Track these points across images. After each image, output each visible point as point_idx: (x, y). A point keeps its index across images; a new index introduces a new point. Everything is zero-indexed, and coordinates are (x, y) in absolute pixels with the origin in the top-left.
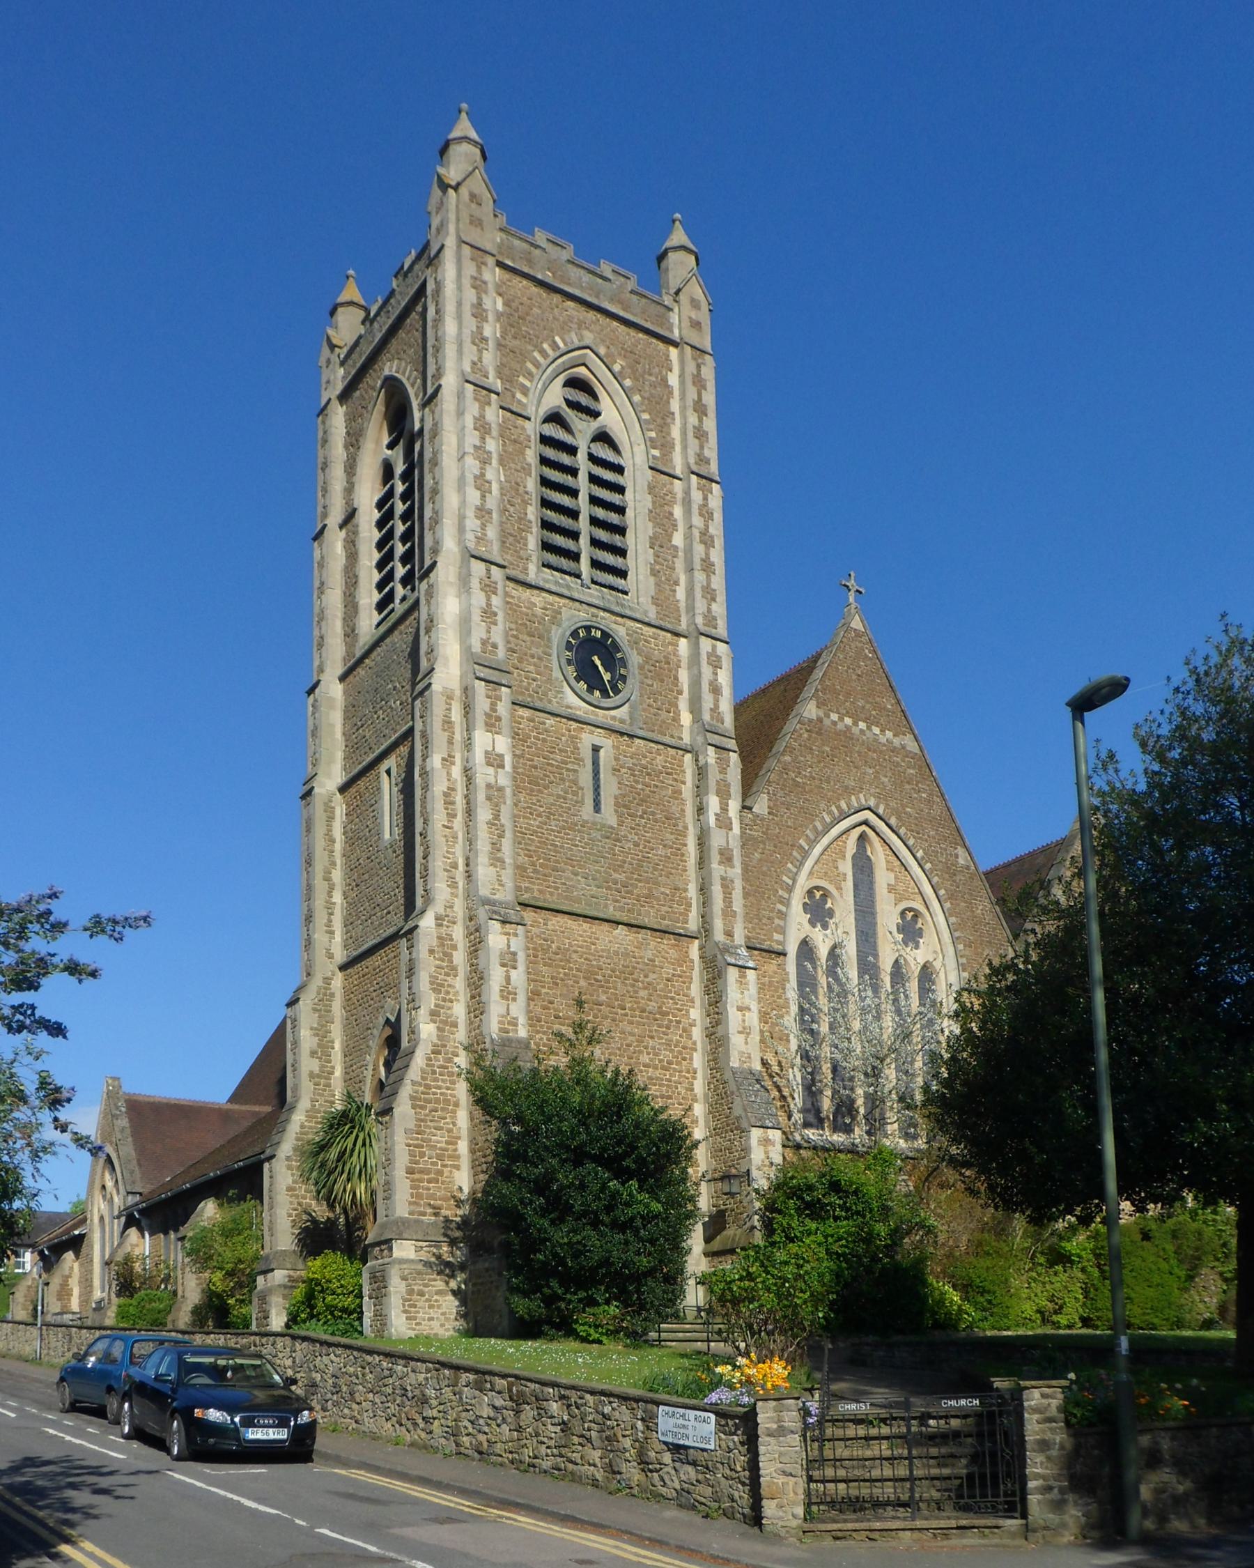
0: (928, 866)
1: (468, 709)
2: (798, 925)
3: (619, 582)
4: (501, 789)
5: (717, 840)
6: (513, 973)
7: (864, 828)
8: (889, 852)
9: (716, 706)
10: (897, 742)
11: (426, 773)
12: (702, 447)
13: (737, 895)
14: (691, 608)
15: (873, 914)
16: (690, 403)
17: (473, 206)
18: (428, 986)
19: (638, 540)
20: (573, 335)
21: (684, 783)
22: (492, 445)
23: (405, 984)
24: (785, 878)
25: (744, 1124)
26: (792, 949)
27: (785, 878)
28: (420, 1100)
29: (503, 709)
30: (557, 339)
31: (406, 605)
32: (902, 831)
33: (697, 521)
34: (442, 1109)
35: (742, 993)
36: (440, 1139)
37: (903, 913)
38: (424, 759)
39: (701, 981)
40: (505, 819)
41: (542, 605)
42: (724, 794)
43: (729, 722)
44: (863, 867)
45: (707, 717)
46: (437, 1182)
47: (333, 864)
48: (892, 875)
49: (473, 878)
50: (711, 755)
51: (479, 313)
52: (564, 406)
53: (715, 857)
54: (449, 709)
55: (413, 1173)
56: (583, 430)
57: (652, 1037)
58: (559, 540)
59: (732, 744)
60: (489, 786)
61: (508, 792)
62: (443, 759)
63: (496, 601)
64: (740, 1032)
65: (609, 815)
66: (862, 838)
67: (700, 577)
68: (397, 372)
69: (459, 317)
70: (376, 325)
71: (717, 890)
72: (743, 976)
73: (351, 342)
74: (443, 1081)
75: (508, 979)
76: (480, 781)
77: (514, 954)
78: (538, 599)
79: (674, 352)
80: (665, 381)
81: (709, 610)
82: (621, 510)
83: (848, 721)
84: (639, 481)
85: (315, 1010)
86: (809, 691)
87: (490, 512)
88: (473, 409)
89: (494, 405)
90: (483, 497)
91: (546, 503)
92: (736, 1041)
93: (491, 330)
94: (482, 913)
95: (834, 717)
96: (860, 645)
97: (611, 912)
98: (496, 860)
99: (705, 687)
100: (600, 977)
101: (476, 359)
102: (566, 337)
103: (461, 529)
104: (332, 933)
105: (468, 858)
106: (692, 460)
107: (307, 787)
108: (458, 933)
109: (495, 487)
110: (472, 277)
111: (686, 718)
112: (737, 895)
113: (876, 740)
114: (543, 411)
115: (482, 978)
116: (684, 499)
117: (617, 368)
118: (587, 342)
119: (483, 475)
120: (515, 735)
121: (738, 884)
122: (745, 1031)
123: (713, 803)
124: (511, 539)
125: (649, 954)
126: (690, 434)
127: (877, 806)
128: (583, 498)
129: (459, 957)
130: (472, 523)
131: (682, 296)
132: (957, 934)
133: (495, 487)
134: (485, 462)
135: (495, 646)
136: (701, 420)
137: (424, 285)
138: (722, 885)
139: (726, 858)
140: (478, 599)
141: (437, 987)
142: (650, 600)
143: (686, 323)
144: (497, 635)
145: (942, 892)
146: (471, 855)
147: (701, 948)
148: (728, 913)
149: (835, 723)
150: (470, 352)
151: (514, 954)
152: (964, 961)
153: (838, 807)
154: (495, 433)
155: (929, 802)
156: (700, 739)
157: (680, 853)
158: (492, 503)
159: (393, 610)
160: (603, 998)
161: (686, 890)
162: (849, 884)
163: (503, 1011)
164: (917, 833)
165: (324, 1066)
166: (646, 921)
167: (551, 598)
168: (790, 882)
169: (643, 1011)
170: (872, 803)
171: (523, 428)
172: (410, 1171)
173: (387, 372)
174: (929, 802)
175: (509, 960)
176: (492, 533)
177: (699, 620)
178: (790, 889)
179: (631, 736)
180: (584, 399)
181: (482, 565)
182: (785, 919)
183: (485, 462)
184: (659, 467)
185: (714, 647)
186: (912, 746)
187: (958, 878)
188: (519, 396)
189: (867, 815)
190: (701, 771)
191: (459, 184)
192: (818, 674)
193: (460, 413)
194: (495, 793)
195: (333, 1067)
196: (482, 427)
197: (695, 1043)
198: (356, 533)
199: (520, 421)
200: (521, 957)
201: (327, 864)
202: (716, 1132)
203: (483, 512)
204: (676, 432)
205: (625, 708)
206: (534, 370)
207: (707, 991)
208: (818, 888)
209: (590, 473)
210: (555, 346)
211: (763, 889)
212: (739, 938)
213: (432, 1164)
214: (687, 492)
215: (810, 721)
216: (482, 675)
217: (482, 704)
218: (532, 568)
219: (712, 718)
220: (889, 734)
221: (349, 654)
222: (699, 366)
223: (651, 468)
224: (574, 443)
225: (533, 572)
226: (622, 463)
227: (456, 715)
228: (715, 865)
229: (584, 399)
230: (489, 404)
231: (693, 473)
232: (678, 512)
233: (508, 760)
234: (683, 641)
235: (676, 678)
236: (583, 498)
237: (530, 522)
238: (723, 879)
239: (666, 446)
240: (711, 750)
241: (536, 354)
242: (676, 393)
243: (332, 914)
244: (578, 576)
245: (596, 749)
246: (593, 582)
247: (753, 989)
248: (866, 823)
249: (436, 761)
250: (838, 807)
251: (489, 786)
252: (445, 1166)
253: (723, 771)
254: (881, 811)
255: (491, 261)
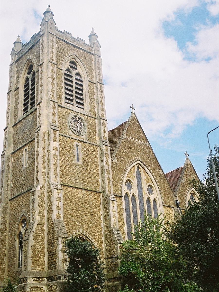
0: (153, 174)
1: (49, 136)
2: (125, 190)
3: (82, 107)
4: (57, 156)
5: (106, 168)
6: (60, 202)
7: (138, 165)
8: (144, 171)
9: (105, 136)
10: (144, 144)
11: (38, 151)
12: (100, 77)
13: (111, 182)
14: (98, 113)
15: (141, 186)
16: (97, 67)
17: (51, 25)
18: (38, 206)
19: (86, 97)
20: (72, 52)
21: (98, 154)
22: (55, 75)
23: (31, 206)
24: (121, 178)
25: (116, 243)
26: (123, 195)
27: (121, 178)
28: (35, 237)
29: (57, 136)
30: (68, 53)
31: (32, 110)
32: (147, 166)
33: (99, 93)
34: (41, 240)
35: (113, 207)
36: (40, 248)
37: (148, 186)
38: (38, 148)
39: (103, 204)
40: (58, 163)
41: (65, 112)
42: (107, 157)
43: (107, 140)
44: (139, 174)
45: (103, 138)
46: (39, 260)
47: (9, 173)
48: (145, 176)
49: (50, 178)
50: (104, 148)
51: (52, 47)
52: (70, 67)
53: (106, 172)
54: (44, 136)
55: (33, 258)
56: (74, 72)
57: (91, 219)
58: (69, 97)
59: (109, 145)
60: (54, 155)
61: (58, 156)
62: (43, 148)
63: (56, 111)
64: (113, 218)
65: (80, 162)
66: (138, 167)
67: (100, 106)
68: (31, 58)
69: (48, 48)
70: (26, 48)
71: (106, 181)
72: (113, 203)
73: (19, 51)
74: (41, 232)
75: (58, 205)
76: (52, 154)
77: (60, 198)
78: (65, 110)
79: (93, 56)
80: (91, 63)
81: (102, 113)
82: (82, 90)
83: (134, 139)
84: (86, 84)
85: (3, 212)
86: (124, 132)
87: (54, 91)
88: (51, 68)
89: (56, 67)
90: (53, 87)
91: (66, 89)
92: (113, 220)
93: (55, 51)
94: (52, 187)
95: (130, 138)
96: (135, 121)
97: (81, 187)
98: (56, 174)
99: (102, 131)
100: (79, 204)
101: (51, 57)
102: (70, 53)
103: (47, 94)
104: (8, 191)
105: (48, 173)
106: (98, 80)
107: (3, 153)
108: (45, 192)
109: (56, 85)
110: (51, 40)
111: (98, 138)
112: (111, 182)
113: (140, 144)
114: (65, 69)
115: (52, 204)
116: (96, 88)
117: (81, 59)
118: (74, 54)
119: (53, 82)
120: (61, 143)
121: (111, 179)
122: (114, 217)
123: (105, 159)
124: (58, 96)
125: (90, 197)
126: (97, 74)
127: (141, 160)
128: (74, 87)
129: (45, 198)
130: (50, 93)
131: (94, 45)
132: (161, 191)
133: (56, 85)
134: (53, 79)
135: (55, 121)
136: (99, 71)
137: (39, 40)
138: (108, 180)
139: (108, 173)
140: (52, 110)
141: (40, 206)
142: (89, 111)
143: (95, 51)
144: (56, 119)
145: (157, 181)
146: (49, 172)
147: (102, 195)
148: (109, 186)
149: (131, 139)
150: (50, 56)
151: (60, 198)
152: (163, 198)
153: (133, 160)
154: (56, 73)
155: (152, 158)
156: (101, 144)
157: (97, 170)
158: (55, 88)
159: (28, 111)
160: (80, 209)
161: (99, 181)
162: (136, 179)
163: (57, 213)
164: (151, 167)
165: (4, 227)
166: (90, 189)
167: (67, 110)
168: (122, 178)
169: (89, 212)
170: (140, 159)
171: (61, 72)
172: (32, 258)
173: (28, 58)
174: (152, 158)
175: (59, 200)
176: (55, 95)
177: (100, 116)
178: (122, 180)
179: (85, 143)
180: (74, 66)
181: (53, 102)
182: (121, 188)
183: (53, 79)
184: (91, 81)
185: (104, 122)
186: (148, 145)
187: (160, 177)
188: (60, 65)
189: (139, 162)
190: (102, 151)
191: (48, 21)
192: (126, 128)
193: (47, 69)
194: (55, 157)
195: (6, 228)
196: (53, 72)
197: (102, 221)
198: (18, 93)
199: (60, 71)
200: (62, 198)
201: (7, 173)
202: (107, 245)
203: (53, 91)
204: (94, 73)
205: (84, 136)
206: (63, 59)
207: (104, 207)
208: (129, 180)
209: (65, 78)
210: (68, 55)
211: (117, 180)
212: (112, 193)
213: (38, 255)
214: (97, 87)
215: (125, 139)
216: (53, 128)
217: (52, 135)
218: (63, 103)
219: (104, 139)
220: (143, 142)
221: (15, 121)
222: (98, 59)
223: (89, 81)
224: (72, 75)
225: (64, 104)
226: (82, 80)
227: (46, 137)
228: (106, 175)
229: (74, 66)
230: (54, 67)
231: (98, 82)
232: (95, 91)
233: (58, 149)
234: (96, 120)
235: (95, 129)
236: (74, 87)
237: (63, 93)
238: (108, 178)
239: (92, 77)
240: (104, 146)
241: (64, 56)
242: (94, 65)
243: (8, 186)
244: (73, 105)
245: (77, 146)
246: (76, 106)
247: (116, 207)
248: (139, 164)
249: (40, 149)
250: (133, 160)
251: (54, 155)
252: (41, 256)
253: (107, 151)
254: (142, 161)
255: (55, 37)
